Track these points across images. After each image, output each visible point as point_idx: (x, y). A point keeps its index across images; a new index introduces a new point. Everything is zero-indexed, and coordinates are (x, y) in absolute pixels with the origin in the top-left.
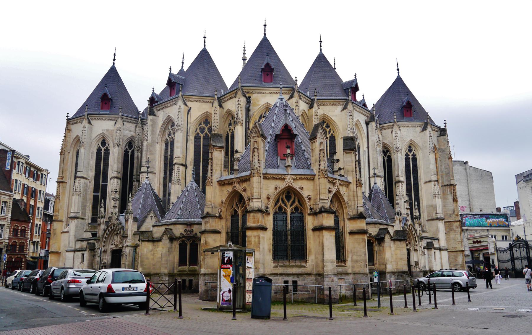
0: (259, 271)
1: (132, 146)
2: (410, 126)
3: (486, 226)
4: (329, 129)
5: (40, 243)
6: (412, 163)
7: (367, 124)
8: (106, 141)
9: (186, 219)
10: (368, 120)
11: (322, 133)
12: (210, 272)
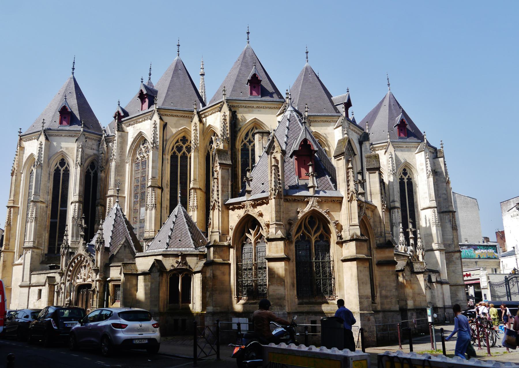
0: (284, 309)
1: (94, 167)
2: (405, 146)
3: (474, 257)
6: (407, 188)
7: (361, 143)
8: (65, 160)
9: (176, 249)
10: (361, 139)
11: (350, 149)
12: (219, 311)
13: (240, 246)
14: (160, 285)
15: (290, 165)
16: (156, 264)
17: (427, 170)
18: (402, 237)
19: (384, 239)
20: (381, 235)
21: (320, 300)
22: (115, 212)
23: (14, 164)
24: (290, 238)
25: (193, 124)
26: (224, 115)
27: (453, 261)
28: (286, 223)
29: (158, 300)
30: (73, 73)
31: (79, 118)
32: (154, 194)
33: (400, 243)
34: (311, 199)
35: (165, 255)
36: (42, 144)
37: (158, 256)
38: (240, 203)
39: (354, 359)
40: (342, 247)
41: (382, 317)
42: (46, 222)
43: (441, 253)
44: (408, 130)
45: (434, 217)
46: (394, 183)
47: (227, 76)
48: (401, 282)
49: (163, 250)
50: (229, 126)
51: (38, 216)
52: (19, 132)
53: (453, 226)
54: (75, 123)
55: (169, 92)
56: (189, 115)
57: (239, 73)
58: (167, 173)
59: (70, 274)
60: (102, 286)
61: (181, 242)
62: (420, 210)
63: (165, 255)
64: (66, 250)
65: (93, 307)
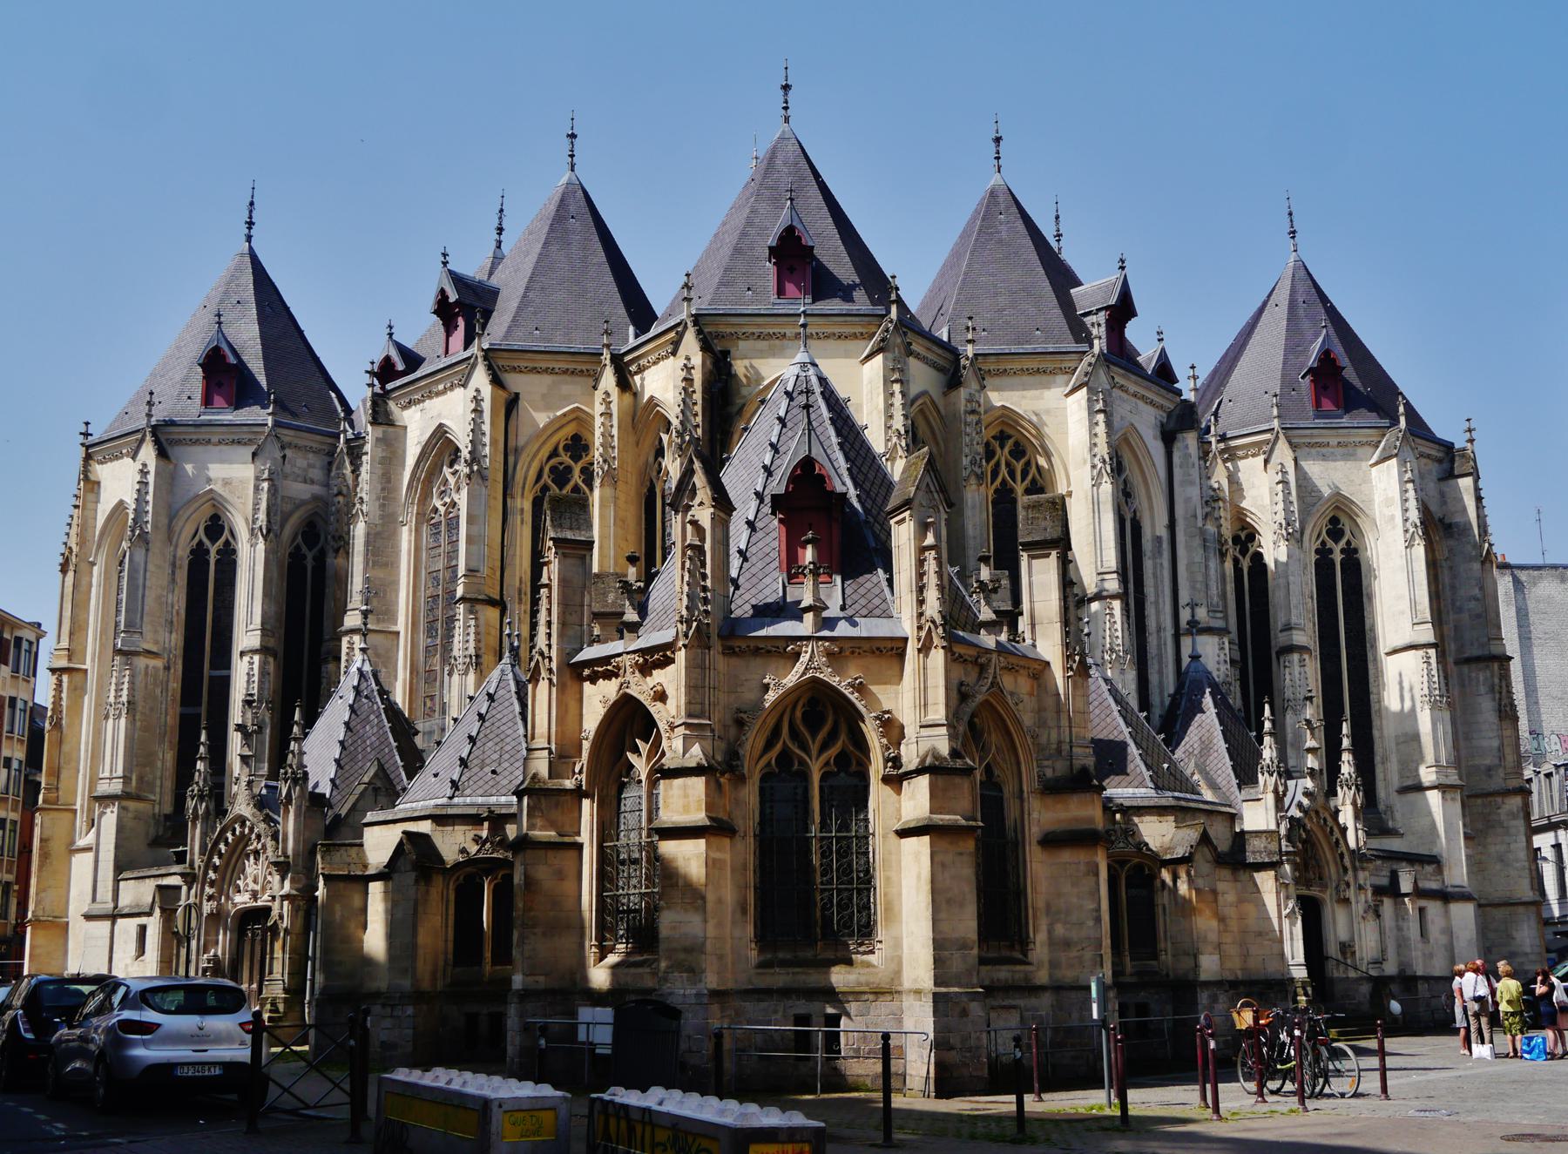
0: (700, 981)
2: (1334, 442)
4: (1023, 461)
5: (16, 887)
7: (1169, 438)
8: (223, 518)
9: (480, 800)
10: (1172, 425)
11: (933, 489)
12: (542, 986)
13: (613, 792)
14: (420, 909)
15: (769, 539)
16: (407, 847)
17: (1406, 520)
18: (1268, 748)
19: (1068, 763)
20: (1059, 751)
21: (830, 955)
22: (355, 683)
23: (68, 534)
24: (737, 766)
25: (599, 395)
26: (685, 365)
27: (1500, 823)
28: (729, 722)
29: (413, 956)
30: (249, 238)
31: (262, 380)
32: (472, 623)
33: (1262, 768)
34: (807, 646)
35: (440, 819)
36: (148, 473)
37: (420, 823)
38: (606, 660)
39: (505, 1107)
40: (899, 791)
41: (1052, 1006)
42: (166, 714)
43: (1448, 796)
44: (1348, 386)
45: (1426, 676)
46: (1291, 568)
47: (716, 235)
48: (1184, 898)
49: (440, 801)
50: (700, 402)
51: (139, 697)
52: (81, 434)
53: (1500, 705)
54: (251, 401)
55: (531, 295)
56: (589, 368)
57: (749, 222)
58: (521, 557)
59: (213, 878)
60: (301, 914)
61: (498, 778)
62: (1383, 656)
63: (440, 819)
64: (204, 804)
65: (272, 977)
